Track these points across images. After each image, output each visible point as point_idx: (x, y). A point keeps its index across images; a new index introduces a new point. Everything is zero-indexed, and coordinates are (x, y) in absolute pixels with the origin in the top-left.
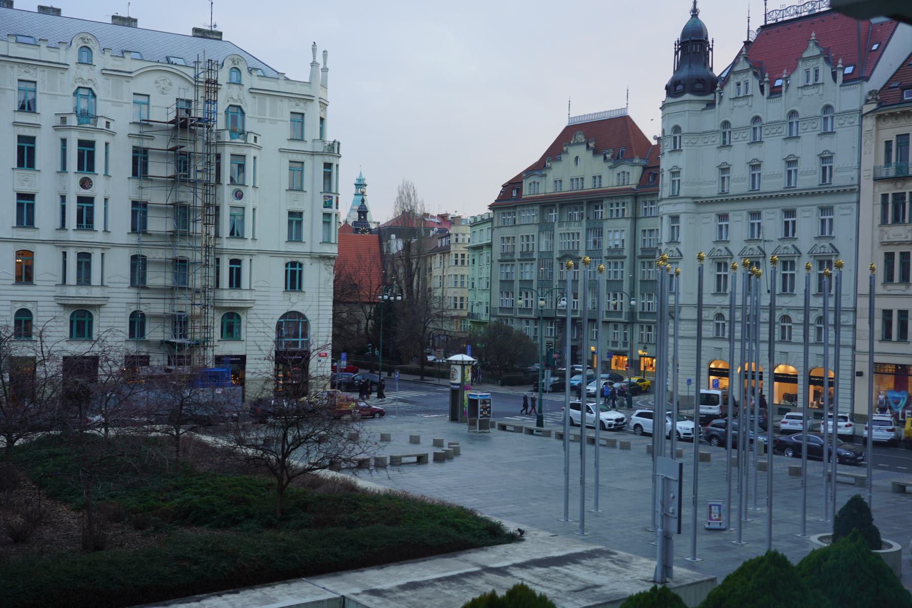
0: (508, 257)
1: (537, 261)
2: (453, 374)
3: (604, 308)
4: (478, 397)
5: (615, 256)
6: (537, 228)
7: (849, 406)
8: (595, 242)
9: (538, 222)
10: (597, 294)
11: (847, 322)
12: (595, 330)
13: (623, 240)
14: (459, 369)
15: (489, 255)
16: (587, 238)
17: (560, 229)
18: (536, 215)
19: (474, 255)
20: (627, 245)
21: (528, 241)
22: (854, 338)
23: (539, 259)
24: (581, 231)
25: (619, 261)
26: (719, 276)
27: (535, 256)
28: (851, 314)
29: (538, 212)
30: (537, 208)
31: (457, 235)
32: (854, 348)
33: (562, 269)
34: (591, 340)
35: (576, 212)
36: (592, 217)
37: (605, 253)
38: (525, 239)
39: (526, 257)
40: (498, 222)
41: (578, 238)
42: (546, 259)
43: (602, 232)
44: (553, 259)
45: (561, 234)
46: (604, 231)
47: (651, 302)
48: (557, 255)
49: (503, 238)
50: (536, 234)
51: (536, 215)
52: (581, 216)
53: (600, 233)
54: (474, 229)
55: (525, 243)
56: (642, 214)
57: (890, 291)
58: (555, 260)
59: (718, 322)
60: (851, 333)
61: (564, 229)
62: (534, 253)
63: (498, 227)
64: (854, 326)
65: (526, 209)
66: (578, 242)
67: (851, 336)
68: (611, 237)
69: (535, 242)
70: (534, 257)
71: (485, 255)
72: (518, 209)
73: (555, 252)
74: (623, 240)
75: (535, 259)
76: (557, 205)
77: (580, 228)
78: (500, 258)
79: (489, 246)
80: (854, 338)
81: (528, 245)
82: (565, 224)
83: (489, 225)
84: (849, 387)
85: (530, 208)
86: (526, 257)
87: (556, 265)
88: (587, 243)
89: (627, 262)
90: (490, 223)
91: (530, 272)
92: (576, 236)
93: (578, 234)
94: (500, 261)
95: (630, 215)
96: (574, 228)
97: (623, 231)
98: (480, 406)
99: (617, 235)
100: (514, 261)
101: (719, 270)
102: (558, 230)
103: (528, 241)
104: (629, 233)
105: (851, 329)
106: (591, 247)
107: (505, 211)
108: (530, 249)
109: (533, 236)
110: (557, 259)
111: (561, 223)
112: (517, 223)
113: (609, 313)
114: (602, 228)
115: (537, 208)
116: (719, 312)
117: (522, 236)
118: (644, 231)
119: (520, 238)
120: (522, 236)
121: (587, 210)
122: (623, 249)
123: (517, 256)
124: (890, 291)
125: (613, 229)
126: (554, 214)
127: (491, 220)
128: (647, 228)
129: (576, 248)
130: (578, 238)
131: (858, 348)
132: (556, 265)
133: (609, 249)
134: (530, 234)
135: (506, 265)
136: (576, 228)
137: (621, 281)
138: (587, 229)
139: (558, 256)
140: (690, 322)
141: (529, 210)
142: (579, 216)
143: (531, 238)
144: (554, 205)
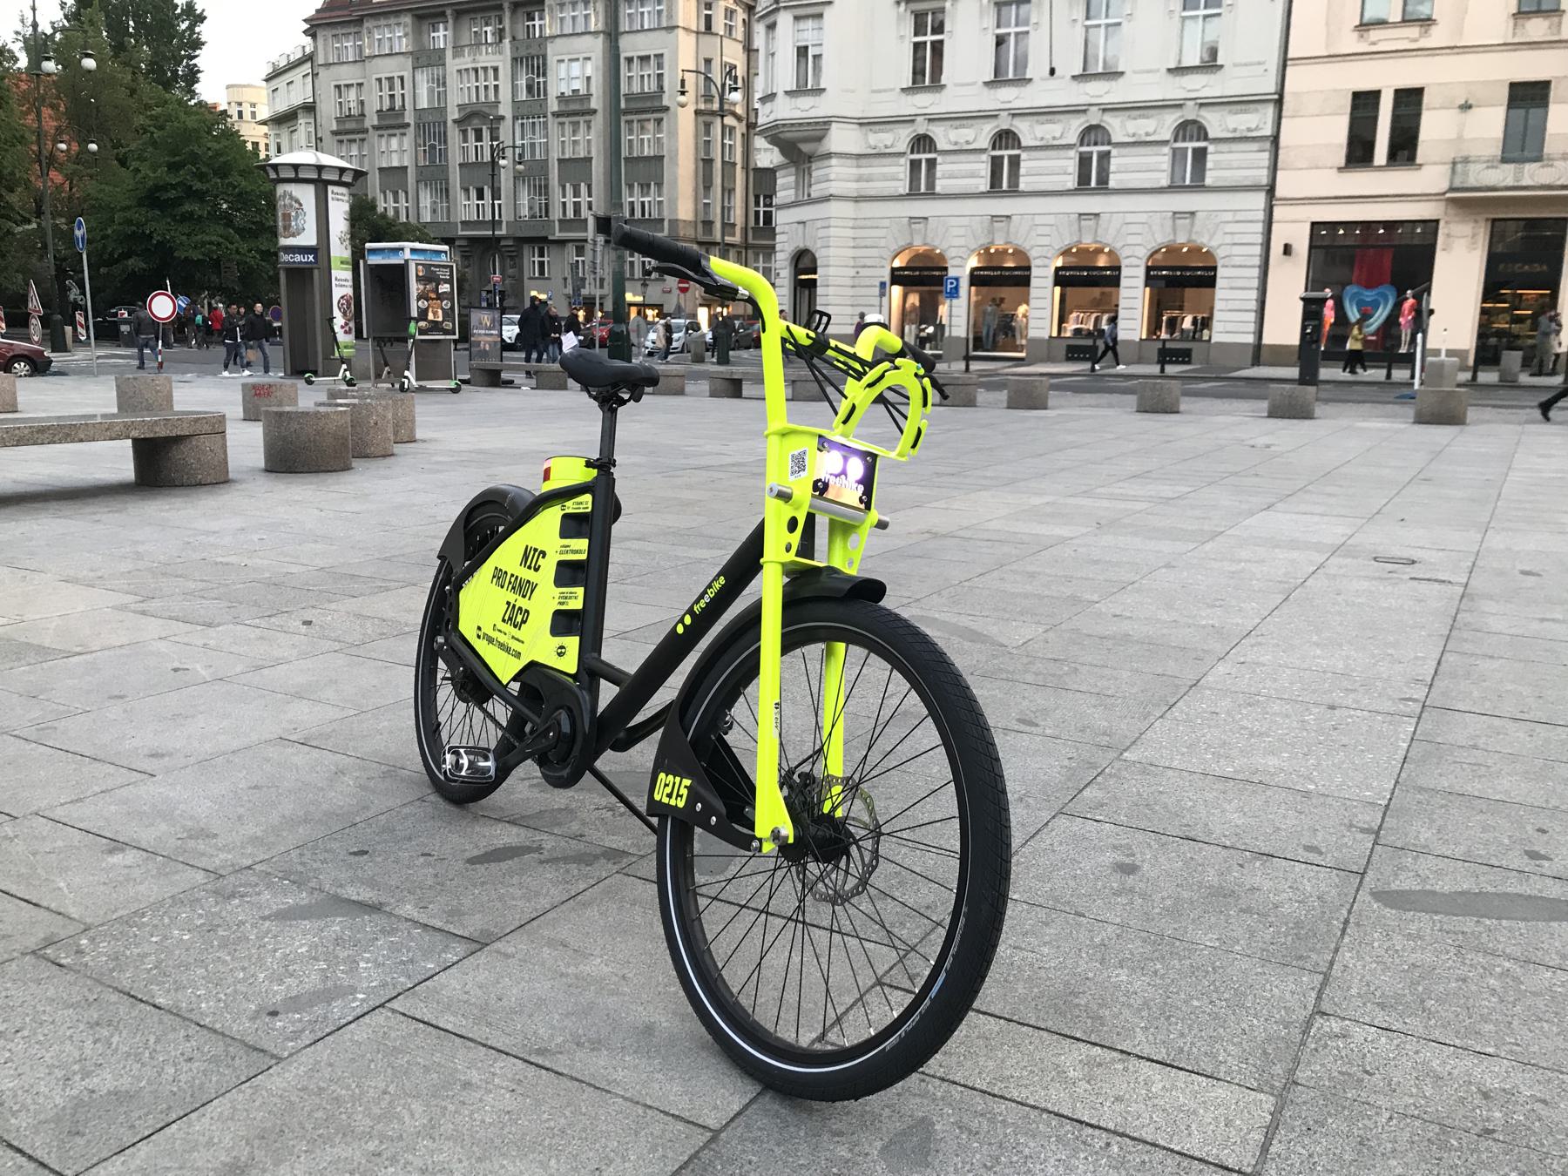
0: (351, 125)
1: (412, 128)
2: (287, 217)
3: (556, 214)
4: (407, 255)
5: (575, 109)
6: (409, 62)
7: (1252, 327)
8: (530, 88)
9: (410, 49)
10: (544, 189)
11: (1257, 128)
12: (536, 259)
13: (589, 78)
14: (306, 195)
15: (313, 130)
16: (514, 78)
17: (457, 61)
18: (406, 35)
19: (278, 135)
20: (597, 89)
21: (391, 88)
22: (1274, 168)
23: (417, 126)
24: (501, 65)
25: (581, 119)
26: (918, 47)
27: (409, 117)
28: (1270, 110)
29: (409, 30)
30: (407, 19)
31: (240, 104)
32: (1271, 190)
33: (465, 140)
34: (530, 278)
35: (489, 29)
36: (521, 35)
37: (553, 106)
38: (385, 84)
39: (391, 121)
40: (326, 54)
41: (496, 78)
42: (431, 127)
43: (545, 64)
44: (445, 123)
45: (459, 71)
46: (549, 62)
47: (646, 199)
48: (453, 114)
49: (338, 87)
50: (407, 75)
51: (406, 35)
52: (500, 34)
53: (542, 70)
54: (274, 84)
55: (386, 92)
56: (624, 25)
57: (1374, 43)
58: (450, 123)
59: (916, 156)
60: (1266, 155)
61: (466, 61)
62: (407, 113)
63: (327, 65)
64: (1275, 139)
65: (383, 22)
66: (496, 87)
67: (1266, 163)
68: (563, 75)
69: (408, 91)
70: (407, 120)
71: (302, 127)
72: (367, 24)
73: (449, 109)
74: (589, 78)
75: (408, 125)
76: (449, 12)
77: (497, 57)
78: (334, 127)
79: (310, 108)
80: (1274, 168)
81: (392, 97)
82: (466, 50)
83: (307, 68)
84: (1255, 283)
85: (392, 21)
86: (391, 121)
87: (454, 134)
88: (514, 88)
89: (598, 122)
90: (309, 65)
91: (398, 151)
92: (491, 73)
93: (496, 69)
94: (335, 133)
95: (600, 27)
96: (486, 58)
97: (589, 59)
98: (414, 288)
99: (576, 69)
100: (366, 131)
101: (919, 29)
102: (452, 64)
103: (391, 88)
104: (600, 63)
105: (1268, 145)
106: (523, 96)
107: (339, 31)
108: (398, 103)
109: (402, 78)
110: (455, 121)
111: (458, 50)
112: (367, 52)
113: (565, 224)
114: (544, 57)
115: (407, 19)
116: (921, 131)
117: (379, 80)
118: (630, 60)
119: (375, 85)
120: (379, 80)
121: (513, 22)
122: (588, 96)
123: (372, 120)
124: (1374, 43)
125: (566, 58)
126: (441, 33)
127: (309, 58)
128: (635, 54)
129: (492, 98)
130: (496, 78)
131: (1279, 193)
132: (454, 134)
133: (562, 98)
134: (395, 75)
135: (351, 141)
136: (491, 57)
137: (589, 160)
138: (514, 60)
139: (456, 116)
140: (849, 162)
141: (388, 26)
142: (493, 34)
143: (397, 83)
144: (443, 14)
